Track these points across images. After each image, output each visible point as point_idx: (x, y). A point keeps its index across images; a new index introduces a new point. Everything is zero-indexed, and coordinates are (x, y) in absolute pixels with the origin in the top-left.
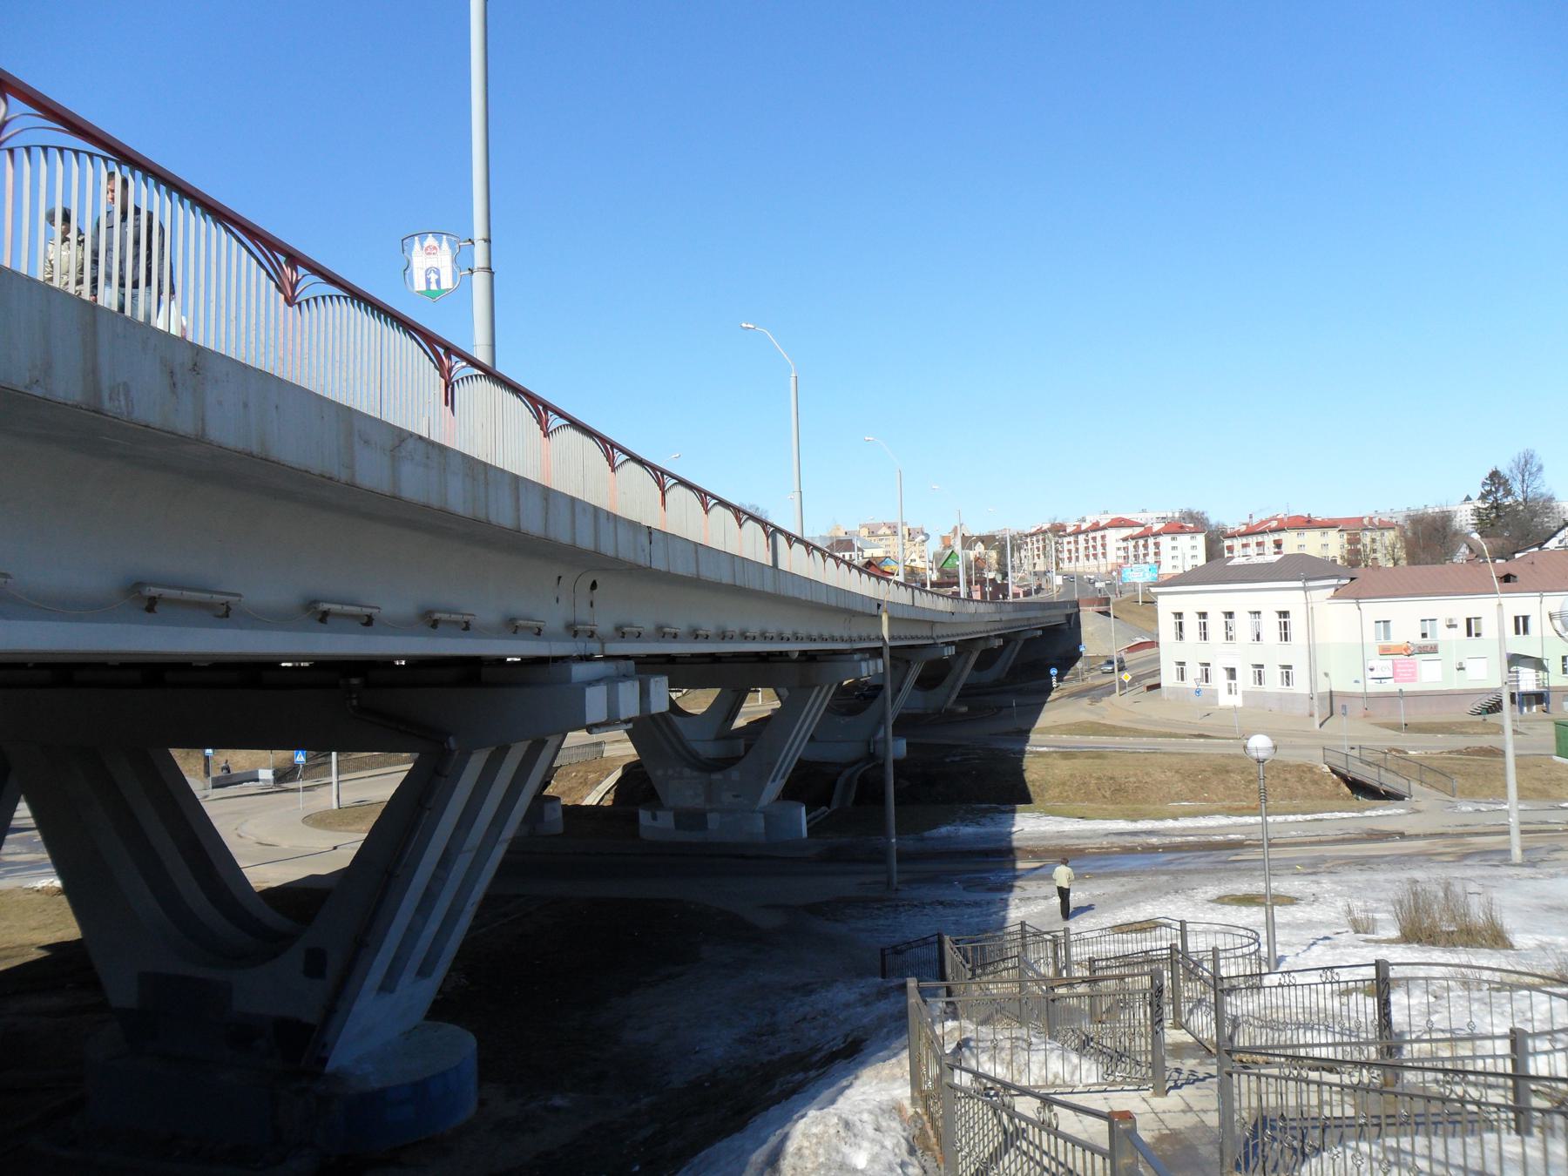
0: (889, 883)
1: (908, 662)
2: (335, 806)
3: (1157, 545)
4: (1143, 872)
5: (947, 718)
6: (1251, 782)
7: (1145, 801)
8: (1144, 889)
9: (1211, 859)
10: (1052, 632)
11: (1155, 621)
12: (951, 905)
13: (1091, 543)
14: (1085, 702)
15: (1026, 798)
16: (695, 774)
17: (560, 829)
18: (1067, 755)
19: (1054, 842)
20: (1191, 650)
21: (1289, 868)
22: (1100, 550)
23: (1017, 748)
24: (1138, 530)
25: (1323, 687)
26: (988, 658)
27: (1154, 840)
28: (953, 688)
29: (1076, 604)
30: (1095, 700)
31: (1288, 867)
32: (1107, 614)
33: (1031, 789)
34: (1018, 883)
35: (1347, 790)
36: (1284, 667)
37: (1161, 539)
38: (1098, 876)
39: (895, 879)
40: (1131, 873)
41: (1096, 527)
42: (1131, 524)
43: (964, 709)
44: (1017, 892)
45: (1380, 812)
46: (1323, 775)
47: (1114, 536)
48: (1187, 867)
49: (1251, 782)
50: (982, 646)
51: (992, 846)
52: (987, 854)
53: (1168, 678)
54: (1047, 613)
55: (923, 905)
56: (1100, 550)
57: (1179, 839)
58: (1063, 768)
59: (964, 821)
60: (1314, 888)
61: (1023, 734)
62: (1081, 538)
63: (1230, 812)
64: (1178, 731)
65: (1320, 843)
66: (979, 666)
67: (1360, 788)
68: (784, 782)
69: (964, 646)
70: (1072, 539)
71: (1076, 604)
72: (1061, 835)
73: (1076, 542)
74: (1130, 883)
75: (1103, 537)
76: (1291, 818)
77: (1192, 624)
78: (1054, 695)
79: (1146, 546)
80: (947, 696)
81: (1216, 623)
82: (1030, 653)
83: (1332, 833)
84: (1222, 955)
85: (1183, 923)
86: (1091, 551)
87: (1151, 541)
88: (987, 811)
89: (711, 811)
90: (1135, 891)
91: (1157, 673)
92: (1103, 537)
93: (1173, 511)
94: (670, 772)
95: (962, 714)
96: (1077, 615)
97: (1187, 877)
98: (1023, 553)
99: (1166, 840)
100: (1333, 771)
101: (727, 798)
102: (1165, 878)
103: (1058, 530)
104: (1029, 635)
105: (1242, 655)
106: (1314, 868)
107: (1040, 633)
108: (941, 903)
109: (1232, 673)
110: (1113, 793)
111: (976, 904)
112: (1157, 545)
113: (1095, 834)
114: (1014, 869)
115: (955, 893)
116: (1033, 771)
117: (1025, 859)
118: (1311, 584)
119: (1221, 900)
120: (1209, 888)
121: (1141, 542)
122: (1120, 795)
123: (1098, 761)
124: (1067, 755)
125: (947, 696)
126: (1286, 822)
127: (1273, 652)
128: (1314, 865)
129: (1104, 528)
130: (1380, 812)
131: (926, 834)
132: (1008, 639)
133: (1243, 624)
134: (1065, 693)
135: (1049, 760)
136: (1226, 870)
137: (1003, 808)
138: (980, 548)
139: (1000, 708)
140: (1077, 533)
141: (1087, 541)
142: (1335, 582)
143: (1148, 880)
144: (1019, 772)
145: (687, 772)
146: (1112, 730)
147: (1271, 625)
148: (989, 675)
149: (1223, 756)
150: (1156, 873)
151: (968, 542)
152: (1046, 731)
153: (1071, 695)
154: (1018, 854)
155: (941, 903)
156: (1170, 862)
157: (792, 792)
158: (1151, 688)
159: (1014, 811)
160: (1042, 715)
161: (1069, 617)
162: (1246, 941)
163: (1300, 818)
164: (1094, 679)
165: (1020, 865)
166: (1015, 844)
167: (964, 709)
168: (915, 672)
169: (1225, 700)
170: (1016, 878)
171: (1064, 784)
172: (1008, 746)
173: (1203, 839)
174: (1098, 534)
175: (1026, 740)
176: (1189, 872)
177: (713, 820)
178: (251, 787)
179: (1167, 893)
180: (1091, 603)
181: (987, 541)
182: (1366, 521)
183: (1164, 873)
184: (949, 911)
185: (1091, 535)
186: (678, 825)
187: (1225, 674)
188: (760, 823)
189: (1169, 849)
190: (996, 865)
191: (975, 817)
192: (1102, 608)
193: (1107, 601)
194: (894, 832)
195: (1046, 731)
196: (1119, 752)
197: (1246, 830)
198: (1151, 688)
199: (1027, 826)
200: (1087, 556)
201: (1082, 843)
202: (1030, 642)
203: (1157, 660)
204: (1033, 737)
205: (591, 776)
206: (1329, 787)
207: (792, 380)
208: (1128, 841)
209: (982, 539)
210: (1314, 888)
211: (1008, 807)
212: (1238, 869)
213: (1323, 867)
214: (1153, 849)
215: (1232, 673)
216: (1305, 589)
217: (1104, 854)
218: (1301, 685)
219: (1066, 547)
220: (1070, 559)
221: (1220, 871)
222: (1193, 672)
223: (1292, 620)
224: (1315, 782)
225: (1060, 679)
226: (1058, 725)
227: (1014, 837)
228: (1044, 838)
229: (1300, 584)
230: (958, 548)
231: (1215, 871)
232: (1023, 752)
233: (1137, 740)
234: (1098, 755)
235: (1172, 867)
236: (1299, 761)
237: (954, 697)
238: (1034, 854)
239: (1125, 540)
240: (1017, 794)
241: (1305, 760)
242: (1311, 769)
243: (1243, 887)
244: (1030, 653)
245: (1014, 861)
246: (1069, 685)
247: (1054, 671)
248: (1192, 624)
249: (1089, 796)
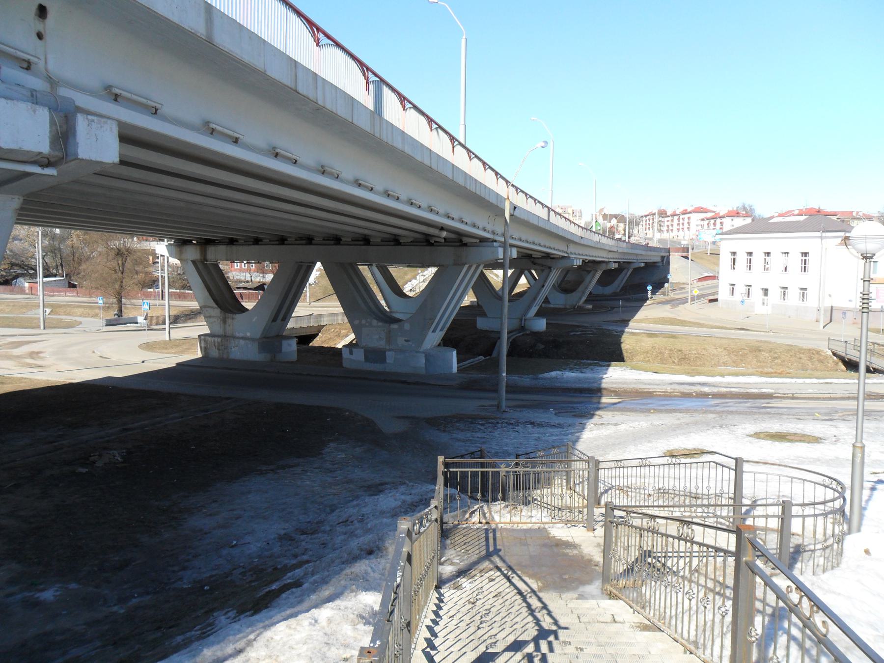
0: (498, 406)
1: (550, 268)
2: (167, 339)
3: (721, 223)
4: (696, 411)
5: (578, 311)
6: (776, 358)
7: (701, 366)
8: (696, 423)
9: (748, 405)
10: (650, 266)
11: (718, 264)
12: (540, 425)
13: (681, 221)
14: (668, 307)
15: (618, 357)
16: (380, 324)
17: (294, 357)
18: (651, 335)
19: (631, 386)
20: (741, 276)
21: (811, 414)
22: (686, 225)
23: (619, 329)
24: (710, 215)
25: (828, 304)
26: (609, 276)
27: (706, 389)
28: (584, 293)
29: (668, 251)
30: (674, 306)
31: (809, 414)
32: (686, 258)
33: (625, 354)
34: (598, 413)
35: (843, 367)
36: (802, 289)
37: (724, 220)
38: (661, 411)
39: (504, 403)
40: (687, 411)
41: (685, 212)
42: (705, 211)
43: (590, 307)
44: (596, 419)
45: (875, 381)
46: (826, 357)
47: (696, 217)
48: (731, 409)
49: (776, 358)
50: (604, 267)
51: (586, 386)
52: (581, 391)
53: (723, 294)
54: (649, 253)
55: (517, 423)
56: (686, 225)
57: (725, 390)
58: (648, 343)
59: (571, 369)
60: (834, 431)
61: (626, 322)
62: (676, 218)
63: (763, 374)
64: (728, 326)
65: (831, 399)
66: (602, 282)
67: (852, 365)
68: (443, 333)
69: (589, 265)
70: (670, 218)
71: (668, 251)
72: (638, 382)
73: (672, 221)
74: (685, 418)
75: (689, 218)
76: (808, 381)
77: (741, 259)
78: (648, 302)
79: (715, 224)
80: (579, 298)
81: (758, 259)
82: (637, 277)
83: (840, 393)
84: (795, 510)
85: (739, 461)
86: (681, 226)
87: (718, 221)
88: (590, 364)
89: (390, 350)
90: (688, 424)
91: (716, 293)
92: (689, 218)
93: (734, 205)
94: (364, 322)
95: (589, 310)
96: (668, 257)
97: (730, 417)
98: (640, 227)
99: (715, 390)
100: (834, 354)
101: (401, 341)
102: (713, 416)
103: (663, 214)
104: (636, 266)
105: (774, 280)
106: (829, 416)
107: (643, 265)
108: (532, 423)
109: (766, 292)
110: (680, 360)
111: (560, 426)
112: (721, 223)
113: (663, 383)
114: (599, 403)
115: (549, 416)
116: (627, 343)
117: (609, 396)
118: (824, 234)
119: (757, 435)
120: (747, 426)
121: (712, 221)
122: (684, 360)
123: (671, 340)
124: (651, 335)
125: (579, 298)
126: (804, 383)
127: (795, 279)
128: (829, 414)
129: (690, 213)
130: (875, 381)
131: (541, 376)
132: (623, 266)
133: (776, 261)
134: (656, 301)
135: (639, 337)
136: (760, 413)
137: (601, 363)
138: (614, 221)
139: (613, 308)
140: (674, 215)
141: (679, 219)
142: (842, 234)
143: (699, 417)
144: (619, 343)
145: (375, 322)
146: (683, 323)
147: (795, 261)
148: (609, 290)
149: (757, 341)
150: (705, 412)
151: (605, 217)
152: (641, 321)
153: (658, 303)
154: (604, 392)
155: (532, 423)
156: (717, 405)
157: (447, 342)
158: (711, 301)
159: (609, 366)
160: (639, 313)
161: (663, 257)
162: (830, 494)
163: (815, 381)
164: (672, 295)
165: (604, 400)
166: (604, 385)
167: (590, 307)
168: (554, 277)
169: (760, 310)
170: (598, 409)
171: (647, 352)
172: (611, 328)
173: (742, 390)
174: (686, 216)
175: (627, 325)
176: (731, 412)
177: (390, 357)
178: (132, 326)
179: (714, 427)
180: (677, 250)
181: (621, 218)
182: (854, 214)
183: (711, 412)
184: (536, 429)
185: (682, 216)
186: (367, 359)
187: (761, 292)
188: (422, 361)
189: (716, 396)
190: (585, 401)
191: (580, 367)
192: (684, 254)
193: (687, 250)
194: (505, 368)
195: (641, 321)
196: (686, 335)
197: (776, 386)
198: (711, 301)
199: (615, 375)
200: (678, 230)
201: (652, 388)
202: (637, 270)
203: (717, 286)
204: (631, 324)
205: (343, 332)
206: (830, 364)
207: (463, 41)
208: (687, 389)
209: (616, 216)
210: (834, 431)
211: (607, 363)
212: (769, 413)
213: (836, 416)
214: (705, 395)
215: (766, 292)
216: (821, 237)
217: (668, 396)
218: (812, 300)
219: (666, 223)
220: (668, 231)
221: (755, 413)
222: (740, 289)
223: (810, 258)
224: (821, 361)
225: (653, 293)
226: (646, 323)
227: (604, 381)
228: (625, 383)
229: (818, 234)
230: (600, 220)
231: (752, 413)
232: (623, 332)
233: (700, 329)
234: (673, 336)
235: (718, 409)
236: (810, 347)
237: (584, 299)
238: (616, 393)
239: (703, 220)
240: (616, 355)
241: (815, 347)
242: (818, 353)
243: (775, 426)
244: (637, 277)
245: (600, 397)
246: (659, 296)
247: (649, 288)
248: (741, 259)
249: (663, 361)
